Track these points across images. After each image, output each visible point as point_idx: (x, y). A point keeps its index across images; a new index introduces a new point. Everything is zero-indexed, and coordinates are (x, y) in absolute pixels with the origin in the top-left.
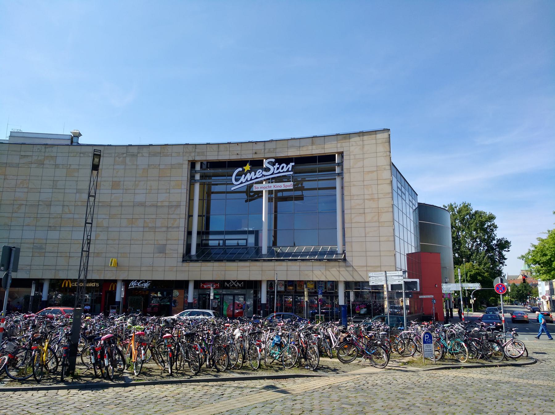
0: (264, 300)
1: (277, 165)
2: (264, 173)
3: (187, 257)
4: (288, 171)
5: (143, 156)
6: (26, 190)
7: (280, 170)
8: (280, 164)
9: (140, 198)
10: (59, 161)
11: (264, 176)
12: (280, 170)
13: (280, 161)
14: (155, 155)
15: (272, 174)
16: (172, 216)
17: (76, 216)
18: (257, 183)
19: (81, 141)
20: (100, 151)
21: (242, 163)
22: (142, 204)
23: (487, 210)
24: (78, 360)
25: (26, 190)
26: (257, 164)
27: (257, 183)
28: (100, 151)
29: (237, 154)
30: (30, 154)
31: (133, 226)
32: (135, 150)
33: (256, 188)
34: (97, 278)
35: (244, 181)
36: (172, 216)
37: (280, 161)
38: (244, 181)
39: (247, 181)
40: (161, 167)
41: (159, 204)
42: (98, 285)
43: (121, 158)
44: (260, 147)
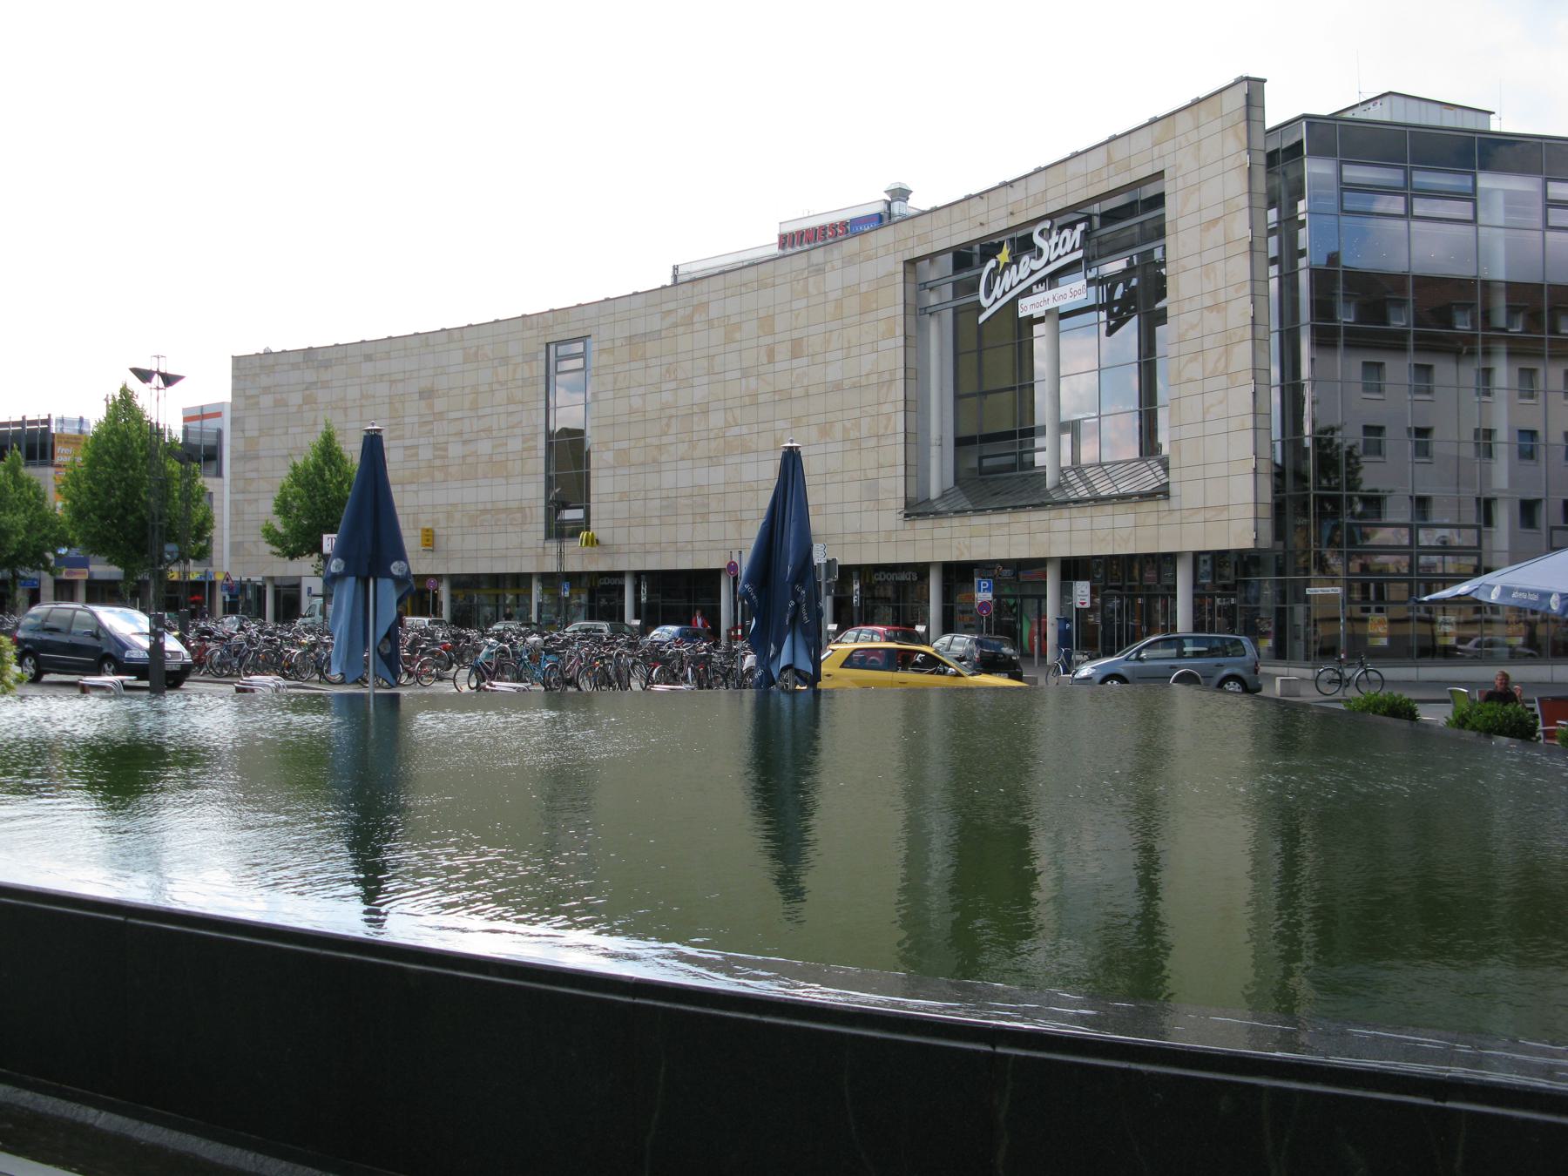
3: (916, 509)
5: (833, 269)
9: (833, 374)
10: (715, 311)
15: (1048, 263)
17: (745, 430)
18: (1024, 294)
19: (918, 202)
20: (548, 345)
22: (838, 387)
27: (1024, 294)
28: (548, 345)
29: (982, 224)
31: (828, 440)
39: (1004, 293)
41: (864, 382)
43: (801, 282)
44: (979, 207)
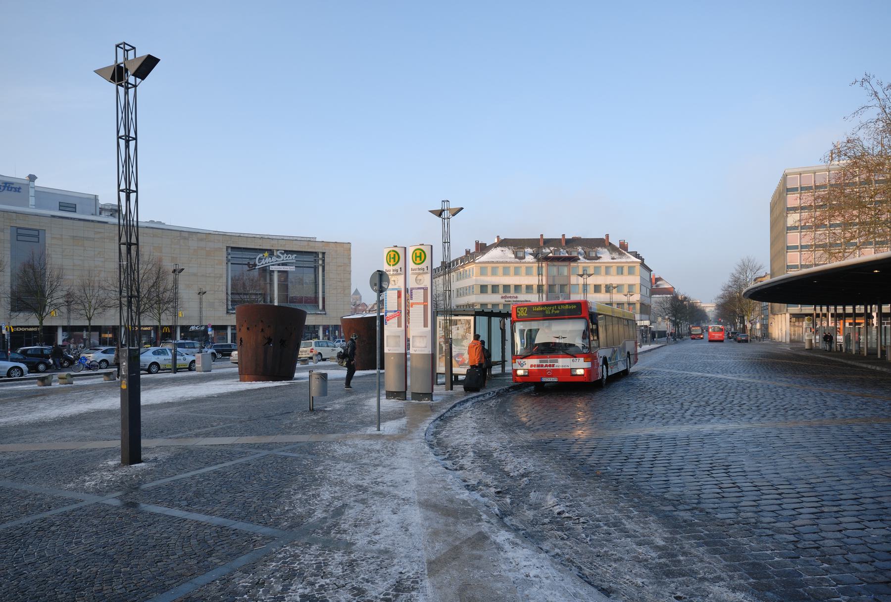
0: (337, 331)
1: (285, 255)
2: (277, 259)
4: (292, 259)
6: (103, 260)
7: (287, 258)
8: (287, 254)
11: (277, 261)
12: (287, 258)
13: (287, 252)
14: (202, 240)
16: (218, 284)
21: (263, 251)
23: (93, 192)
24: (304, 351)
25: (103, 260)
26: (271, 252)
30: (103, 231)
32: (186, 235)
33: (272, 268)
34: (152, 324)
35: (264, 263)
36: (218, 284)
37: (287, 252)
38: (264, 263)
40: (207, 249)
41: (208, 275)
42: (575, 307)
44: (275, 242)
